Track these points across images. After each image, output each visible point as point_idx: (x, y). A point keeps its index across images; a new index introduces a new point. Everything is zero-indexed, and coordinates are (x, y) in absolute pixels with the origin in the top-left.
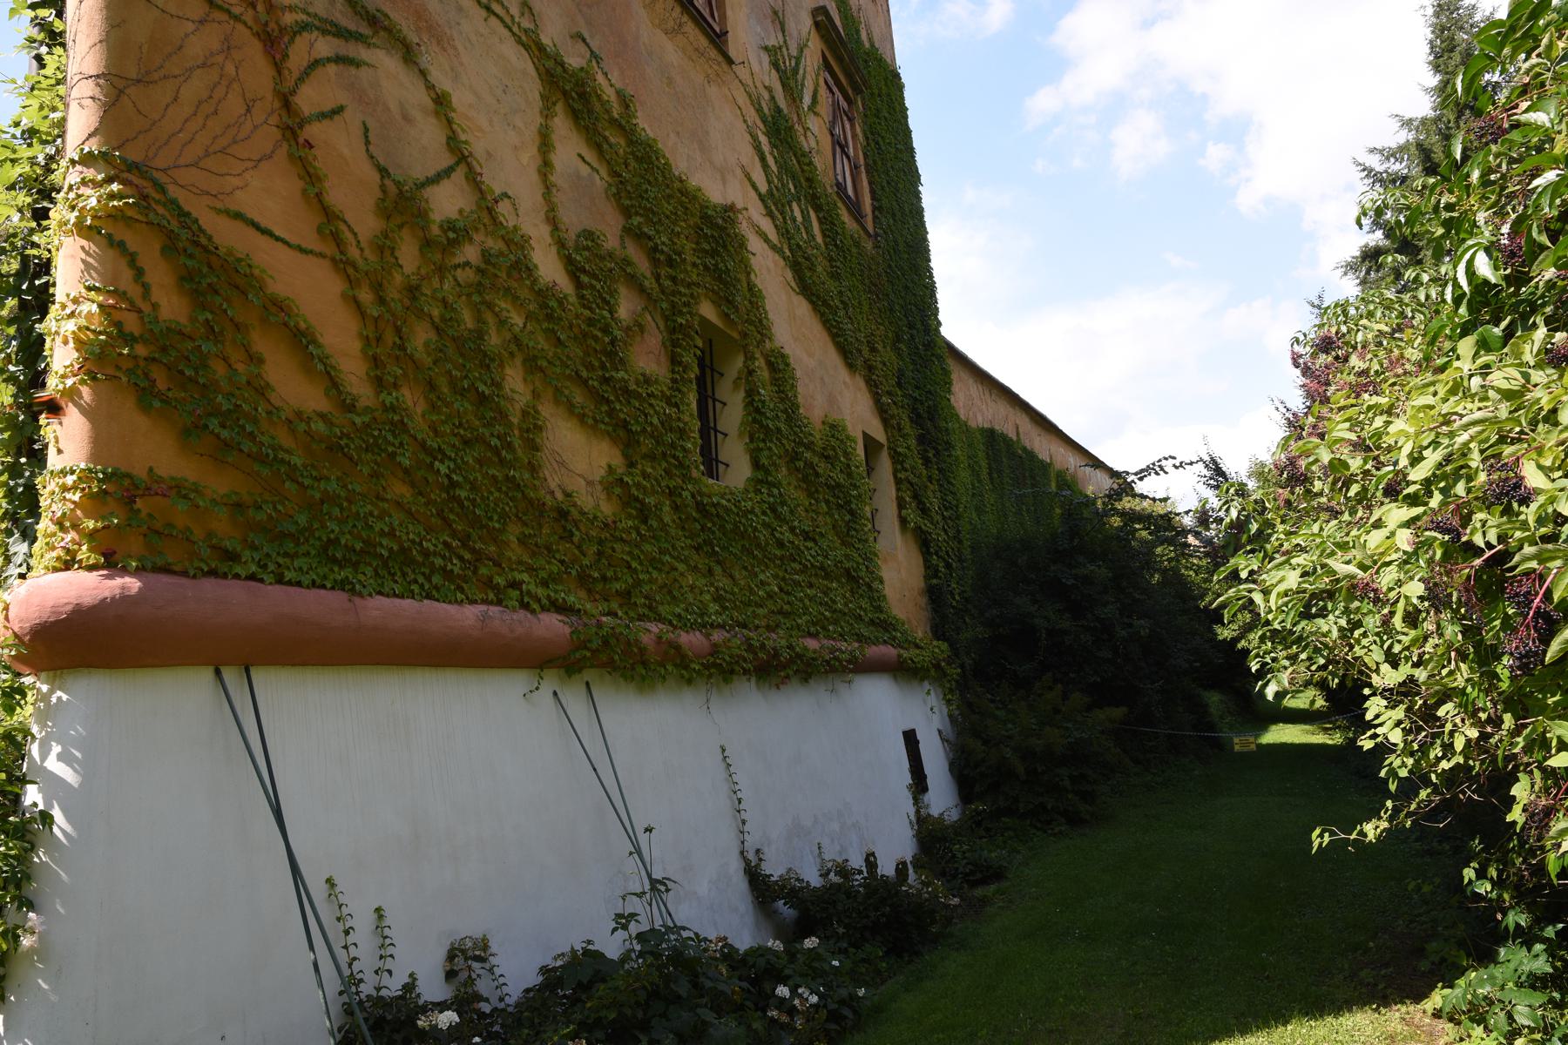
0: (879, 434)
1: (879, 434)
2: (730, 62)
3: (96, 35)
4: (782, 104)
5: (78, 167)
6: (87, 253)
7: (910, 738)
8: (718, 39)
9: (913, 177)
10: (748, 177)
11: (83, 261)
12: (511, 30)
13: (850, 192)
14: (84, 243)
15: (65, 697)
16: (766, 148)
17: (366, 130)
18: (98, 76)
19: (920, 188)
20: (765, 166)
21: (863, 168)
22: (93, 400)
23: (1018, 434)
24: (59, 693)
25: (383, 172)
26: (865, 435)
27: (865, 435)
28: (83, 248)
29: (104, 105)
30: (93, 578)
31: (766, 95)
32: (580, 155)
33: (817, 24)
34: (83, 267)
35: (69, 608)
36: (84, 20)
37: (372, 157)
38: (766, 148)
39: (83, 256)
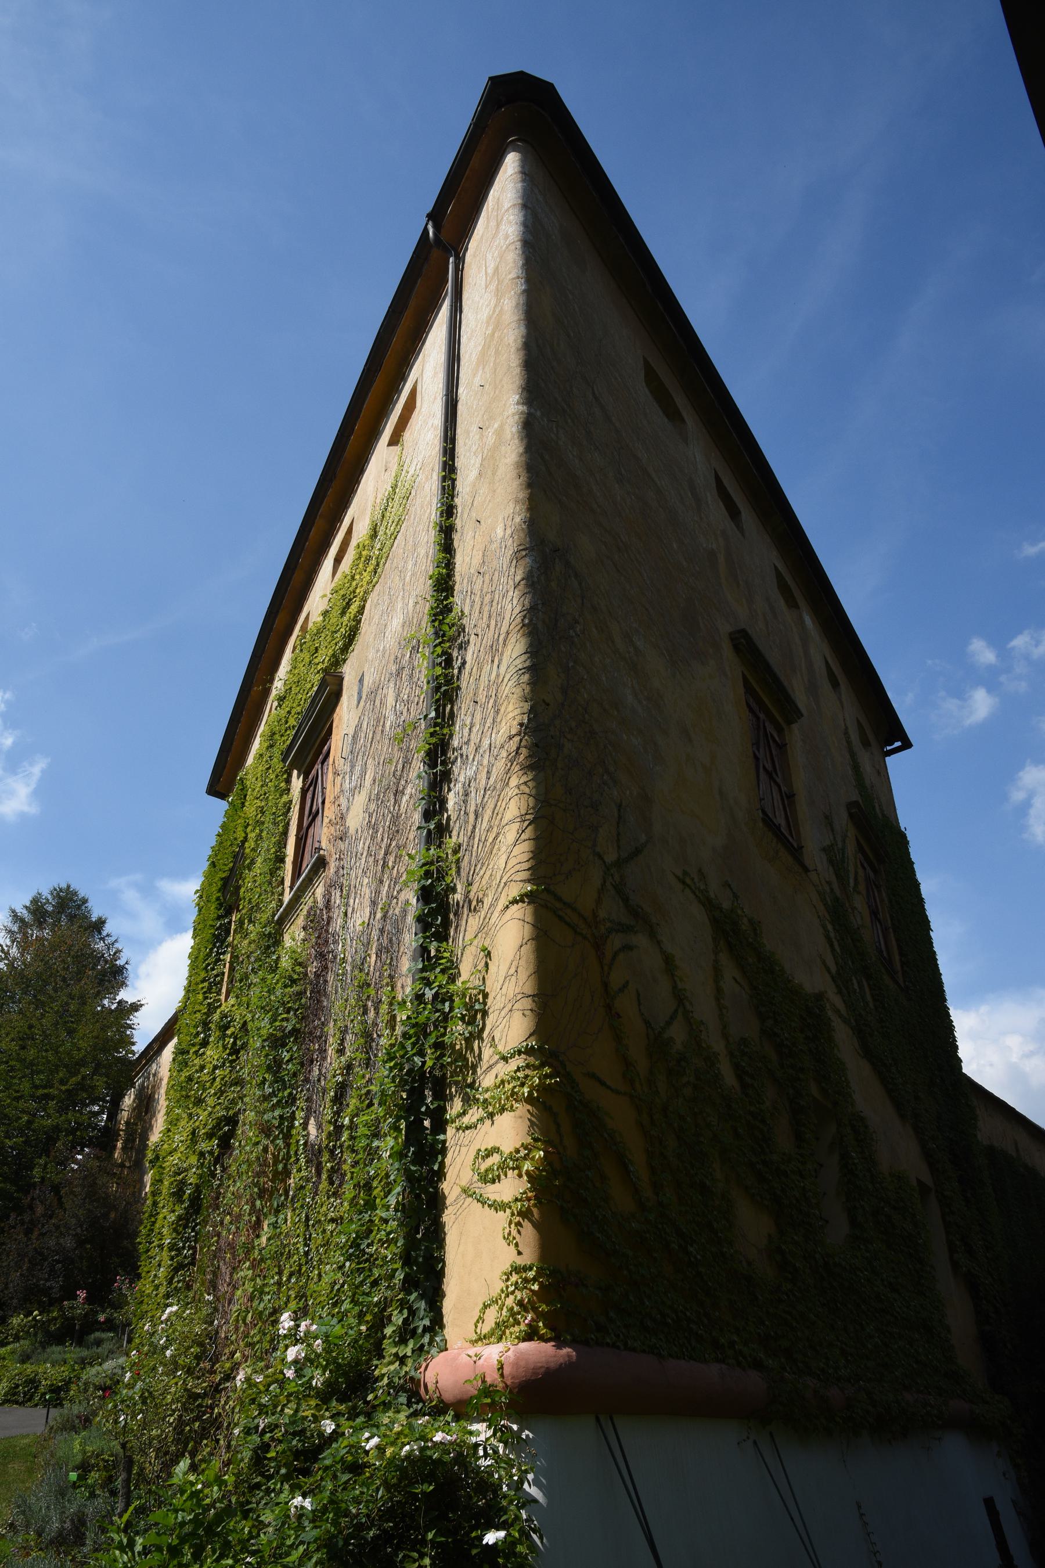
0: (928, 1179)
1: (928, 1179)
2: (806, 870)
3: (531, 970)
4: (838, 892)
5: (523, 1056)
6: (531, 1114)
7: (989, 1503)
8: (796, 852)
9: (924, 925)
10: (824, 962)
11: (529, 1120)
12: (695, 894)
13: (885, 954)
14: (529, 1107)
15: (531, 1436)
16: (832, 935)
17: (638, 995)
18: (534, 996)
19: (931, 933)
20: (833, 950)
21: (891, 930)
22: (540, 1218)
23: (1017, 1150)
24: (527, 1432)
25: (647, 1023)
26: (919, 1181)
27: (919, 1181)
28: (528, 1111)
29: (539, 1014)
30: (548, 1347)
31: (827, 888)
32: (734, 978)
33: (851, 816)
34: (529, 1123)
35: (543, 1370)
36: (524, 959)
37: (643, 1014)
38: (832, 935)
39: (529, 1117)
